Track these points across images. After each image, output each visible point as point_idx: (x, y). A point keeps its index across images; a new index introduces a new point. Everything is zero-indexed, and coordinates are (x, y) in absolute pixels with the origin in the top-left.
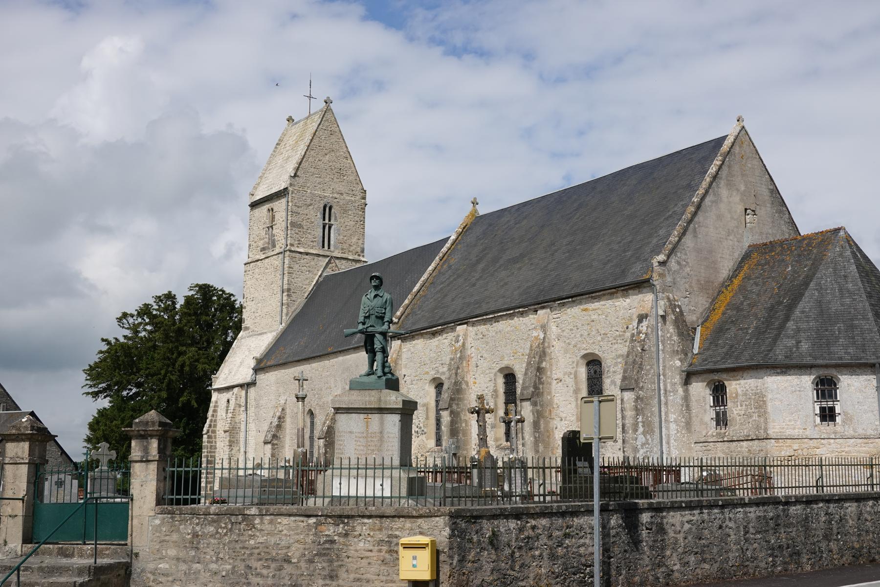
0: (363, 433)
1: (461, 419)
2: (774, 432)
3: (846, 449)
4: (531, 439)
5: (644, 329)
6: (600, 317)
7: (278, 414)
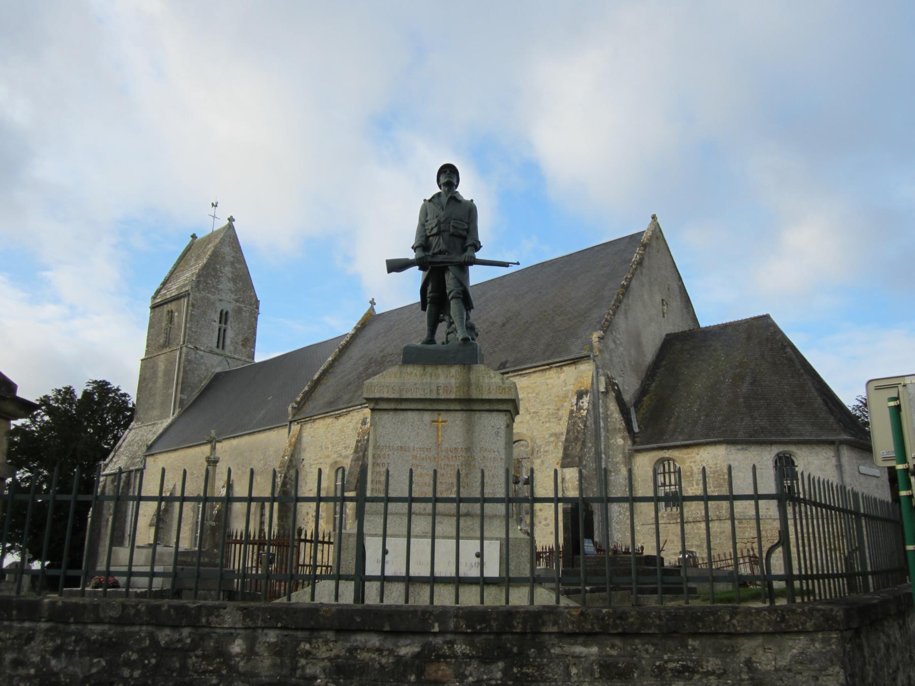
0: (429, 450)
5: (586, 405)
6: (530, 395)
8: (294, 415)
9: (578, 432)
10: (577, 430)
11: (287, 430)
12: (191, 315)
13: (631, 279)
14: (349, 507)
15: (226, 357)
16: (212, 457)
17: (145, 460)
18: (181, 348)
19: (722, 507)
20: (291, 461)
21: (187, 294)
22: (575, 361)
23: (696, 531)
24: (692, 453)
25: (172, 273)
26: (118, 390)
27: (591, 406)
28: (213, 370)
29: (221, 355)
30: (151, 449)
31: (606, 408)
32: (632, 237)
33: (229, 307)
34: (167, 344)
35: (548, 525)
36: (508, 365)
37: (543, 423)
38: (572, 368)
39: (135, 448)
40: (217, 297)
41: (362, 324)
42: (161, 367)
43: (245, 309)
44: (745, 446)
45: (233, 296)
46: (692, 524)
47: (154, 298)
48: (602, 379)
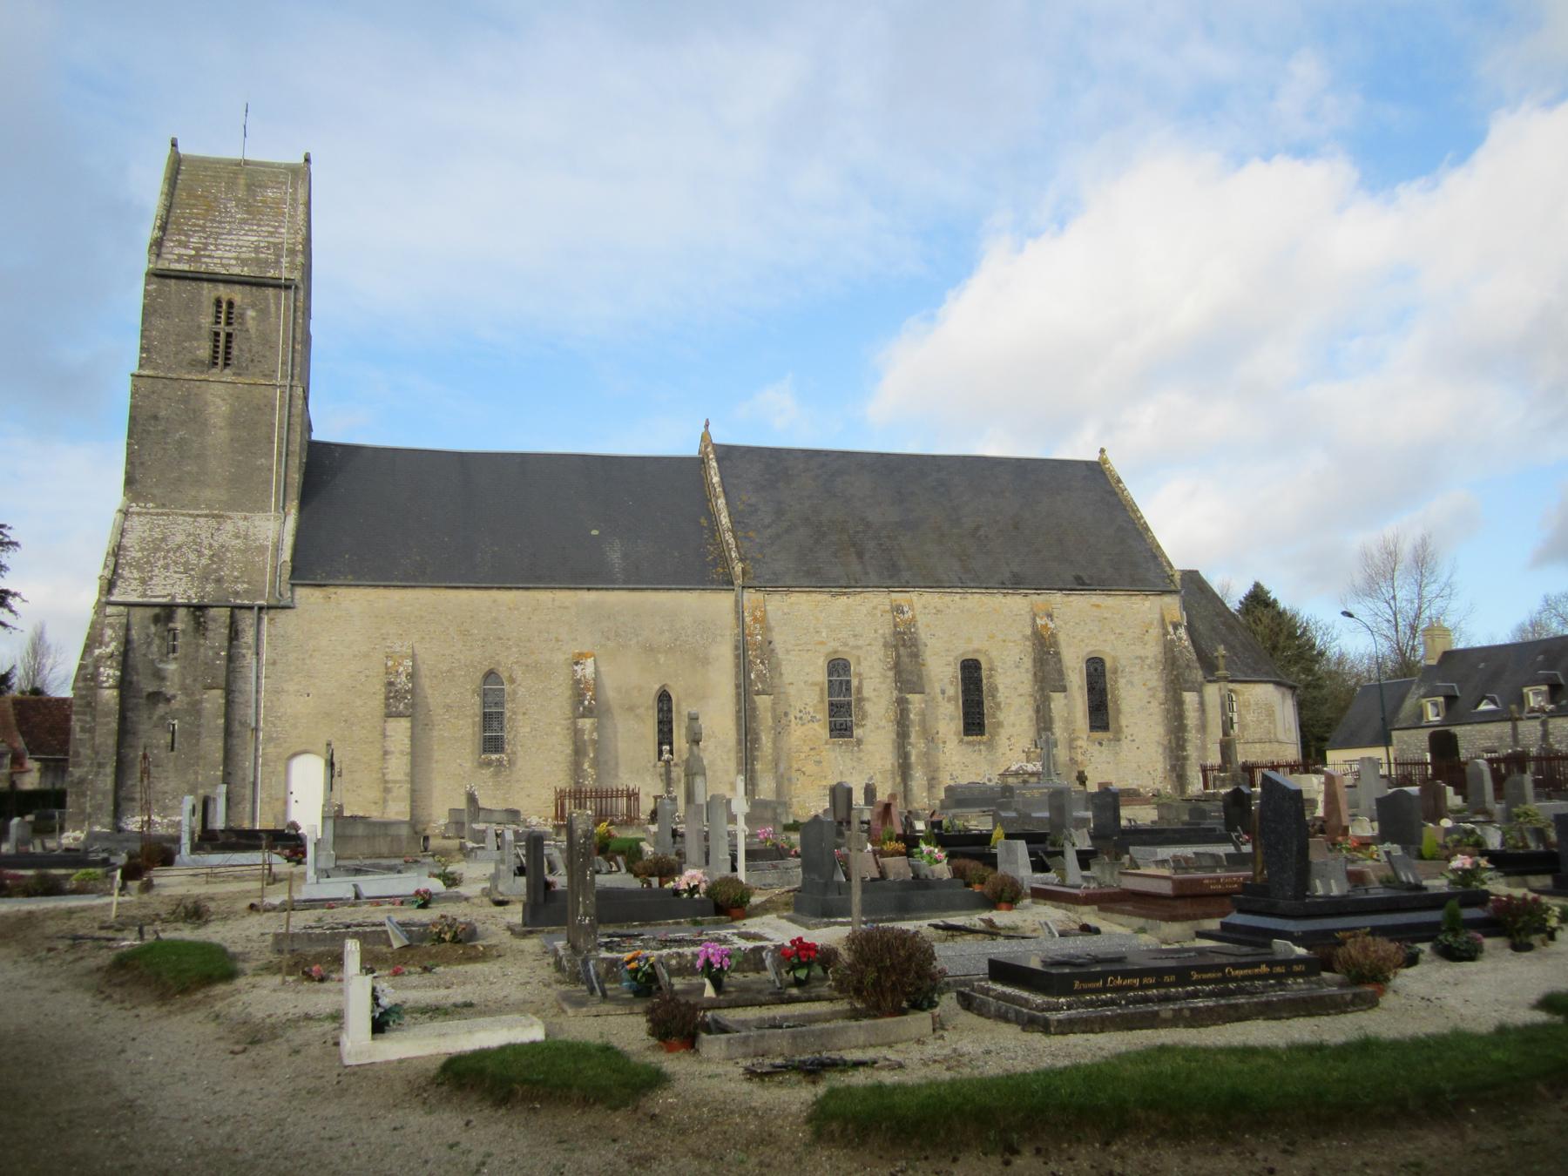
38: (1158, 598)
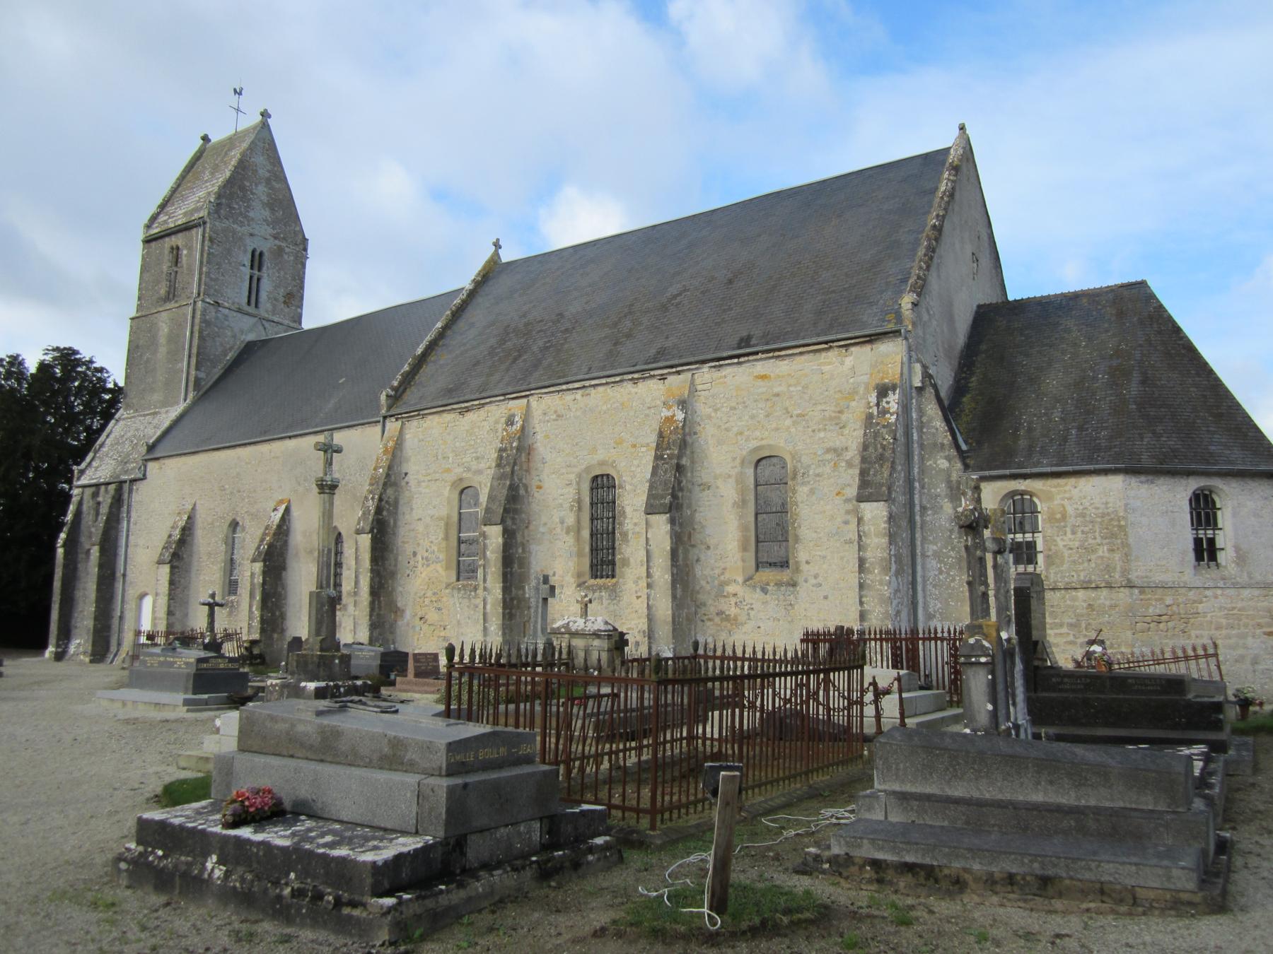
1: (516, 542)
2: (1137, 577)
3: (1239, 605)
4: (666, 576)
5: (894, 407)
6: (792, 389)
7: (181, 524)
8: (389, 408)
9: (884, 447)
10: (882, 444)
11: (378, 428)
12: (209, 254)
13: (944, 216)
14: (491, 548)
15: (262, 319)
16: (328, 478)
17: (145, 467)
18: (195, 302)
19: (1115, 568)
20: (388, 475)
21: (201, 223)
22: (872, 339)
23: (1068, 602)
24: (1066, 484)
25: (174, 191)
26: (91, 362)
27: (900, 409)
28: (243, 337)
29: (255, 316)
30: (153, 450)
31: (921, 412)
32: (926, 158)
33: (265, 246)
34: (171, 296)
35: (821, 585)
36: (753, 341)
37: (814, 431)
38: (867, 348)
39: (127, 448)
40: (245, 230)
41: (484, 276)
42: (164, 329)
43: (287, 250)
44: (1150, 477)
45: (270, 230)
46: (1063, 592)
47: (148, 227)
48: (918, 368)
